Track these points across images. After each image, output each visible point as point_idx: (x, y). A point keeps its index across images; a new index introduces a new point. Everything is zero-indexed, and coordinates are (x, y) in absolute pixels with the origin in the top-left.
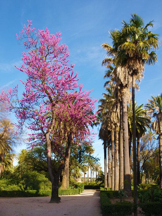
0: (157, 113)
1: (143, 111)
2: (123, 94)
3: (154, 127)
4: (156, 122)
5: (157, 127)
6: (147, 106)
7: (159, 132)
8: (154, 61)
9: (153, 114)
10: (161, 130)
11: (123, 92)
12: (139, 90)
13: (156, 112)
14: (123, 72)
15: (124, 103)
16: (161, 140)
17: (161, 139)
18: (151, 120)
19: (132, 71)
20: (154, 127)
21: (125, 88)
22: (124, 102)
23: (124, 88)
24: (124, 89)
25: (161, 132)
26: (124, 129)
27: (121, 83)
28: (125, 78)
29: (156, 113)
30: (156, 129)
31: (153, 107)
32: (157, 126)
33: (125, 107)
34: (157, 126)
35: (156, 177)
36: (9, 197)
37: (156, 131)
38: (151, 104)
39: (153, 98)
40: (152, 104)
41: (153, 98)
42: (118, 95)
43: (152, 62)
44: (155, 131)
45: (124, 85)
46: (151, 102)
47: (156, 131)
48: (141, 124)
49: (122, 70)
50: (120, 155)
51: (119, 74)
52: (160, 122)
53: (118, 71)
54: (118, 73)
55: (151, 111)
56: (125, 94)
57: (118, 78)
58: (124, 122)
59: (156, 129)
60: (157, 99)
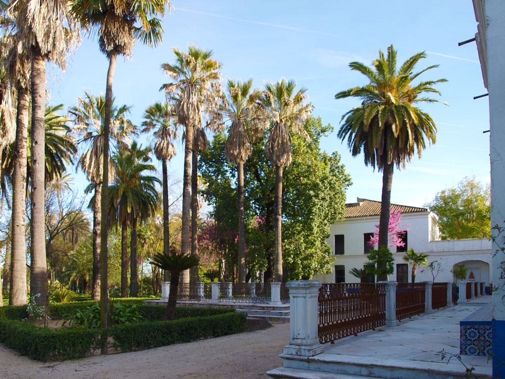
0: (95, 134)
1: (59, 119)
2: (39, 74)
3: (87, 165)
4: (92, 151)
5: (92, 166)
6: (74, 111)
7: (97, 178)
8: (156, 41)
9: (85, 133)
10: (102, 173)
11: (39, 69)
12: (64, 71)
13: (91, 131)
14: (44, 18)
15: (40, 96)
16: (101, 195)
17: (100, 194)
18: (79, 147)
19: (112, 46)
20: (87, 165)
21: (43, 60)
22: (40, 94)
23: (40, 58)
24: (41, 62)
25: (102, 178)
26: (36, 161)
27: (37, 43)
28: (47, 35)
29: (91, 133)
30: (91, 171)
31: (88, 118)
32: (93, 163)
33: (40, 107)
34: (93, 163)
35: (69, 276)
36: (34, 252)
37: (91, 175)
38: (82, 109)
39: (89, 98)
40: (85, 112)
41: (89, 98)
42: (17, 68)
43: (151, 41)
44: (89, 173)
45: (44, 51)
46: (86, 106)
47: (91, 175)
48: (54, 151)
49: (43, 11)
50: (16, 221)
51: (33, 19)
52: (100, 157)
53: (32, 11)
54: (31, 14)
55: (82, 126)
56: (42, 75)
57: (30, 28)
58: (36, 143)
59: (91, 171)
60: (98, 102)
